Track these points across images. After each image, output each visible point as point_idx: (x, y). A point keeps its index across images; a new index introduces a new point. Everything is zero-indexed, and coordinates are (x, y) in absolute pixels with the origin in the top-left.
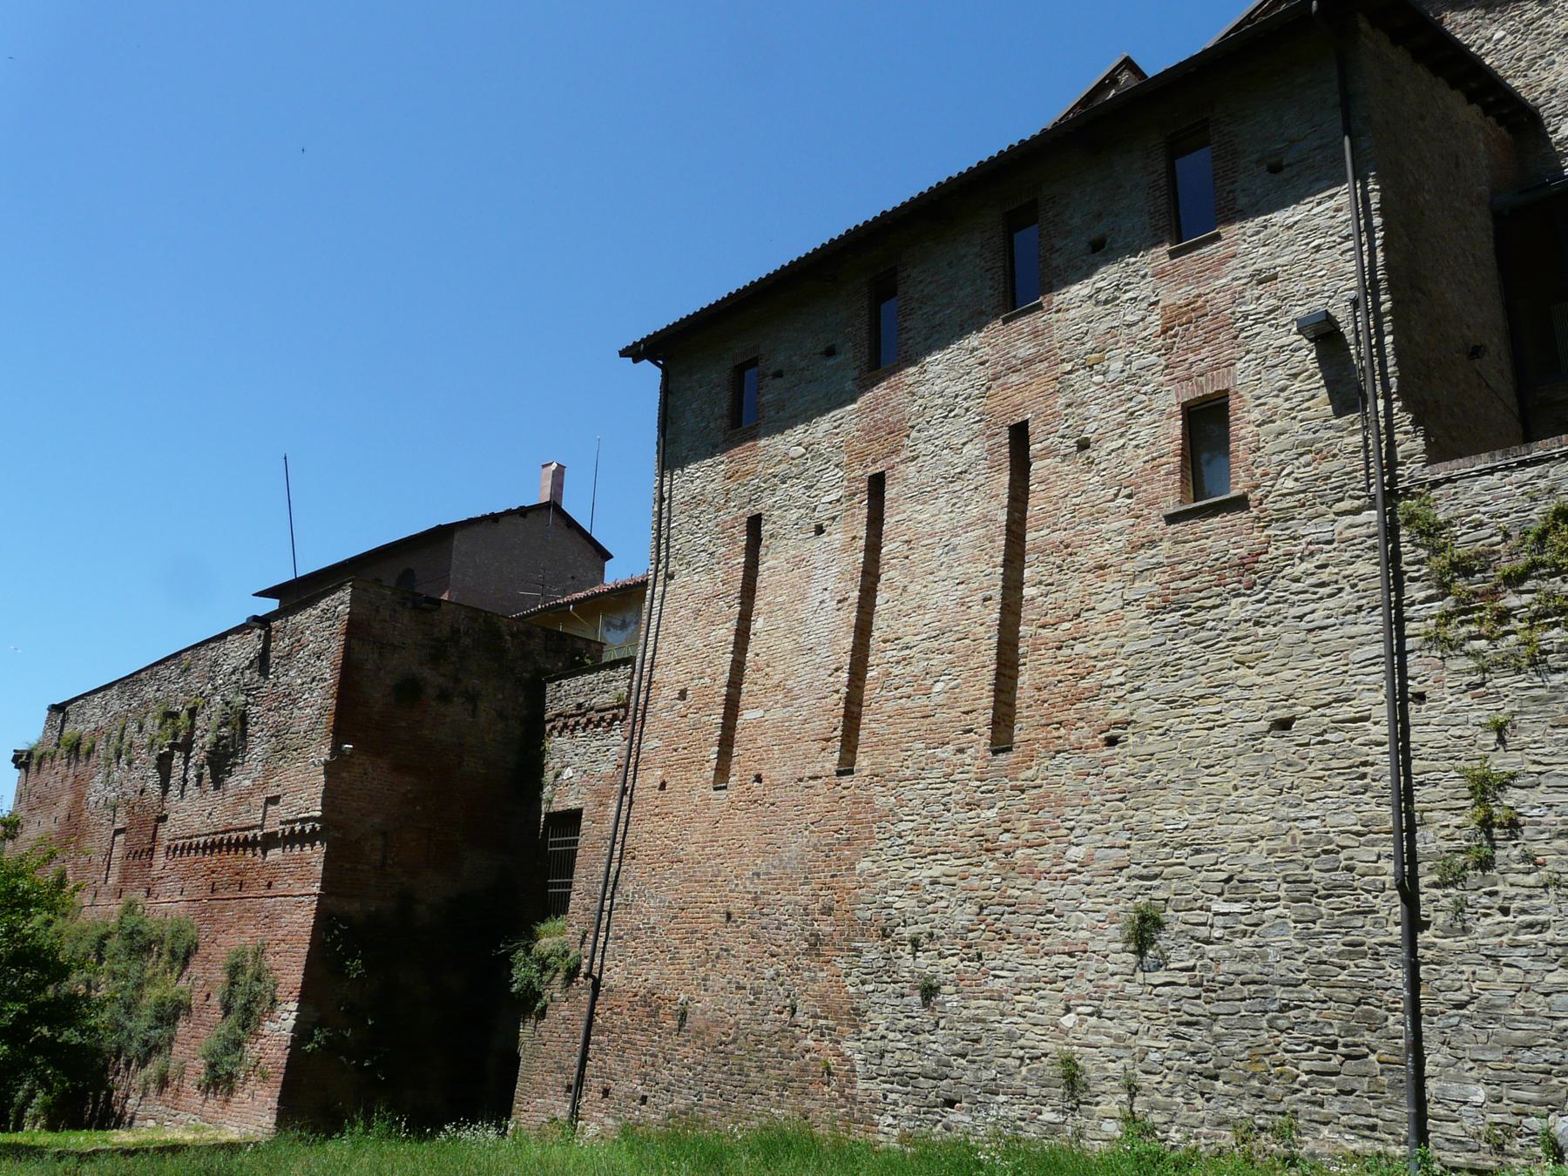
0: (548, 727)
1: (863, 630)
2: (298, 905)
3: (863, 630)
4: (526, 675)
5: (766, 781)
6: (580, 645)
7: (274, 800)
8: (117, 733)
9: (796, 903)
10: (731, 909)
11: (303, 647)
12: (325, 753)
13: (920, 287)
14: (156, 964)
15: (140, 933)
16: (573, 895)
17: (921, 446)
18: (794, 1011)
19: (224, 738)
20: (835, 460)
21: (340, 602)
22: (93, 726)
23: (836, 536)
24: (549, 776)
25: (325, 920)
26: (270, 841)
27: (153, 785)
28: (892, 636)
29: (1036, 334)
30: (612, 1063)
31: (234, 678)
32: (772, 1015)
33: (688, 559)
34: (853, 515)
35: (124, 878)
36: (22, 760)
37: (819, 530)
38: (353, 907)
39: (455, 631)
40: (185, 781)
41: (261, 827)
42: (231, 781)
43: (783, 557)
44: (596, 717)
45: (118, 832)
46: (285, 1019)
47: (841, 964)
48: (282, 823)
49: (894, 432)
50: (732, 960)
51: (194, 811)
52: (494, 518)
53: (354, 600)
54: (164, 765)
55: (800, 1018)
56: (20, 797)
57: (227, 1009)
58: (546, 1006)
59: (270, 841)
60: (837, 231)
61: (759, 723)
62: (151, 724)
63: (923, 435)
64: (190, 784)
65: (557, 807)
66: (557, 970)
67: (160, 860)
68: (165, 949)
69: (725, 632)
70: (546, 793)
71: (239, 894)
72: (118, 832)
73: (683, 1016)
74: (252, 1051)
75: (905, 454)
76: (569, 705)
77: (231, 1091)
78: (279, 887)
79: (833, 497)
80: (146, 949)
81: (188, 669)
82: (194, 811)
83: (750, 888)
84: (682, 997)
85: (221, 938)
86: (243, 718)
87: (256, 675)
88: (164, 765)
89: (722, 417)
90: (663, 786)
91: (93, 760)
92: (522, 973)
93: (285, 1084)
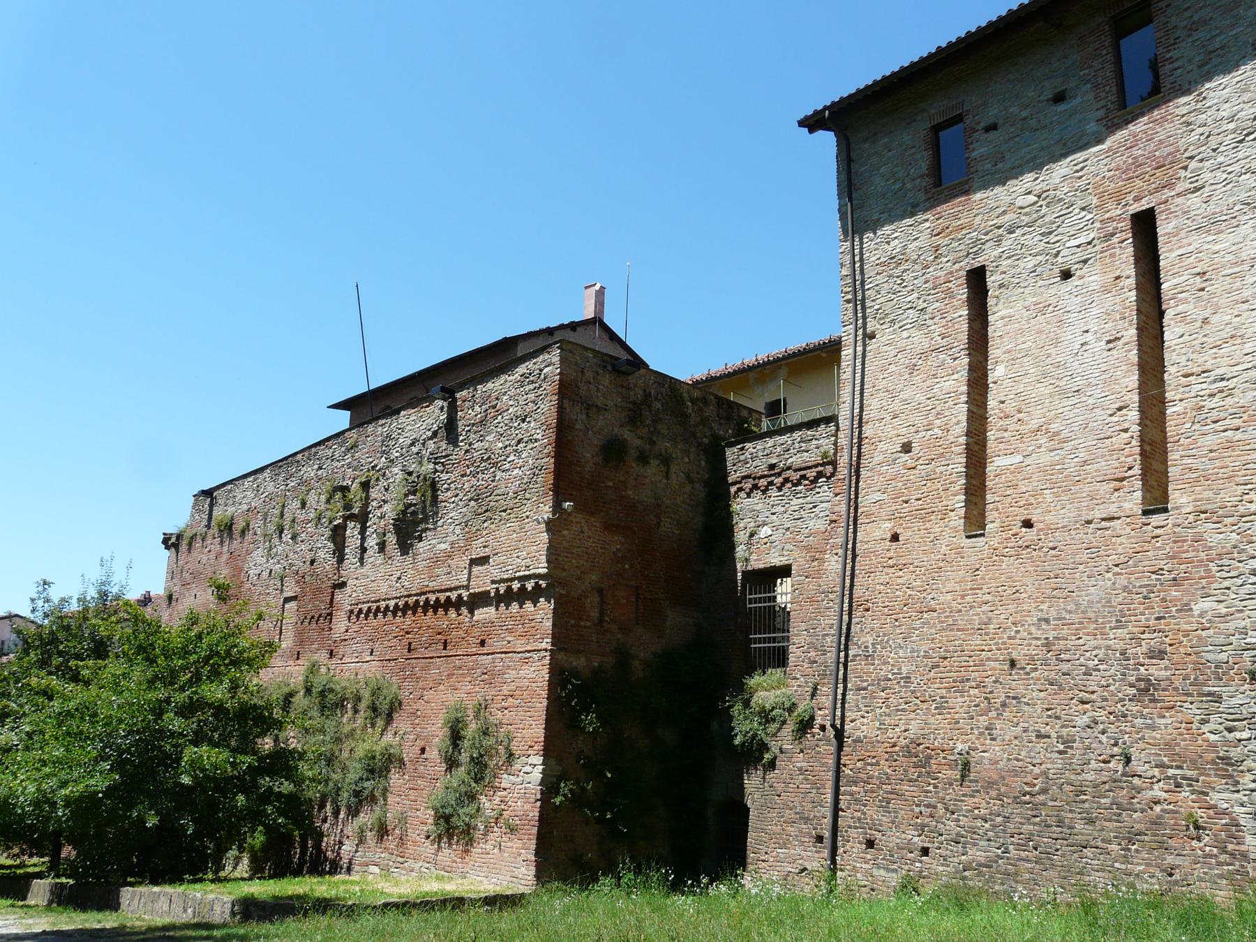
0: (733, 489)
2: (526, 661)
4: (706, 440)
5: (1038, 526)
6: (744, 413)
7: (484, 560)
8: (277, 512)
9: (1108, 648)
10: (1014, 655)
11: (500, 412)
12: (546, 511)
13: (1187, 14)
14: (354, 719)
15: (331, 690)
16: (792, 649)
17: (1207, 176)
18: (1128, 760)
19: (411, 505)
20: (1080, 203)
21: (550, 364)
22: (245, 507)
23: (1091, 278)
24: (740, 536)
25: (559, 676)
26: (480, 600)
27: (325, 553)
28: (1196, 370)
30: (872, 812)
31: (415, 449)
32: (1093, 764)
33: (891, 317)
34: (1112, 255)
35: (301, 640)
36: (172, 542)
37: (1066, 275)
38: (580, 662)
39: (647, 395)
40: (364, 550)
41: (467, 587)
42: (421, 547)
43: (1020, 305)
44: (795, 476)
45: (287, 600)
46: (529, 772)
47: (1193, 711)
48: (493, 582)
49: (1167, 166)
50: (1026, 708)
51: (376, 576)
53: (563, 360)
54: (338, 535)
55: (1136, 766)
56: (172, 575)
57: (452, 764)
58: (775, 758)
59: (480, 600)
62: (316, 500)
63: (1207, 164)
64: (370, 552)
65: (757, 563)
66: (784, 722)
67: (340, 624)
68: (362, 706)
69: (956, 382)
70: (740, 551)
71: (444, 653)
72: (287, 600)
73: (966, 766)
74: (488, 804)
75: (1180, 187)
76: (760, 466)
77: (470, 842)
78: (495, 644)
79: (1083, 240)
80: (340, 705)
81: (354, 446)
82: (376, 576)
83: (1039, 634)
84: (960, 747)
85: (428, 695)
86: (434, 486)
87: (443, 445)
88: (338, 535)
89: (922, 176)
90: (895, 538)
91: (249, 537)
92: (743, 727)
93: (540, 837)
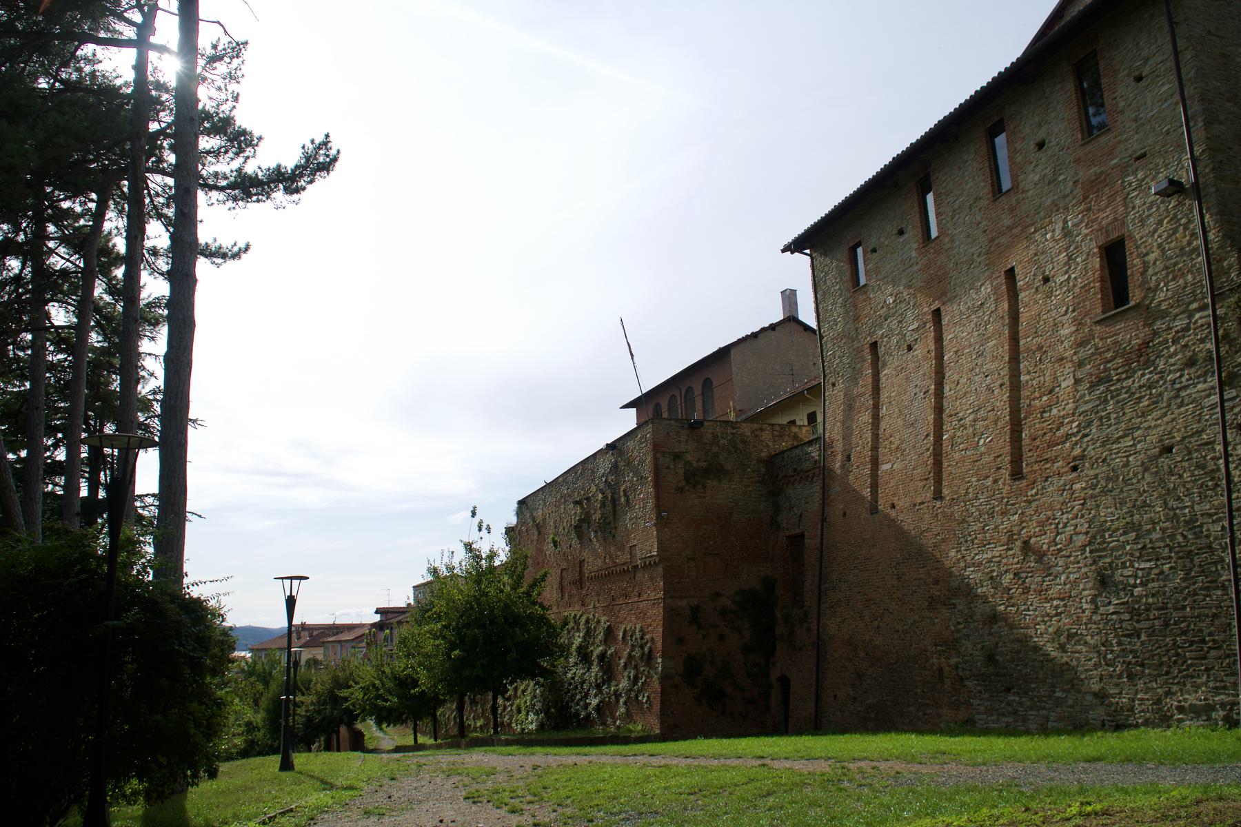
1: (939, 409)
3: (939, 409)
23: (919, 351)
29: (1012, 209)
52: (754, 335)
60: (887, 160)
61: (892, 470)
79: (915, 326)
